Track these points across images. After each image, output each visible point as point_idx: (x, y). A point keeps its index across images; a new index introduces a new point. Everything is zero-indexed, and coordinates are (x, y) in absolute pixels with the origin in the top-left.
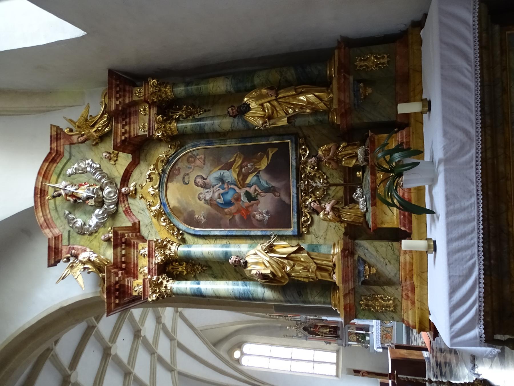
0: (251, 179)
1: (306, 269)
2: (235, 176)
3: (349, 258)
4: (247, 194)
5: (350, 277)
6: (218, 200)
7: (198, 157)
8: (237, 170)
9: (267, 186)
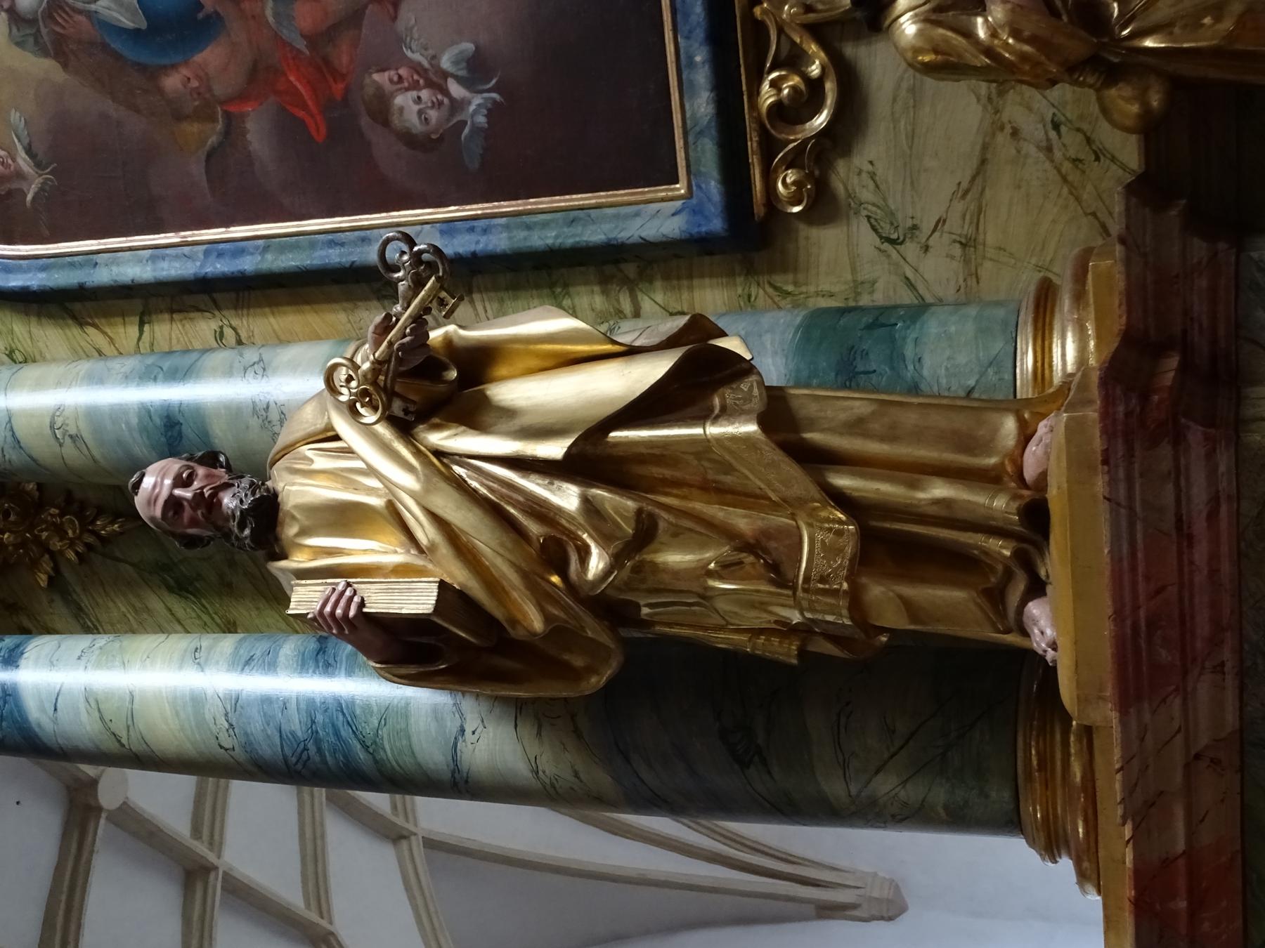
1: (768, 558)
3: (1195, 435)
5: (1203, 626)
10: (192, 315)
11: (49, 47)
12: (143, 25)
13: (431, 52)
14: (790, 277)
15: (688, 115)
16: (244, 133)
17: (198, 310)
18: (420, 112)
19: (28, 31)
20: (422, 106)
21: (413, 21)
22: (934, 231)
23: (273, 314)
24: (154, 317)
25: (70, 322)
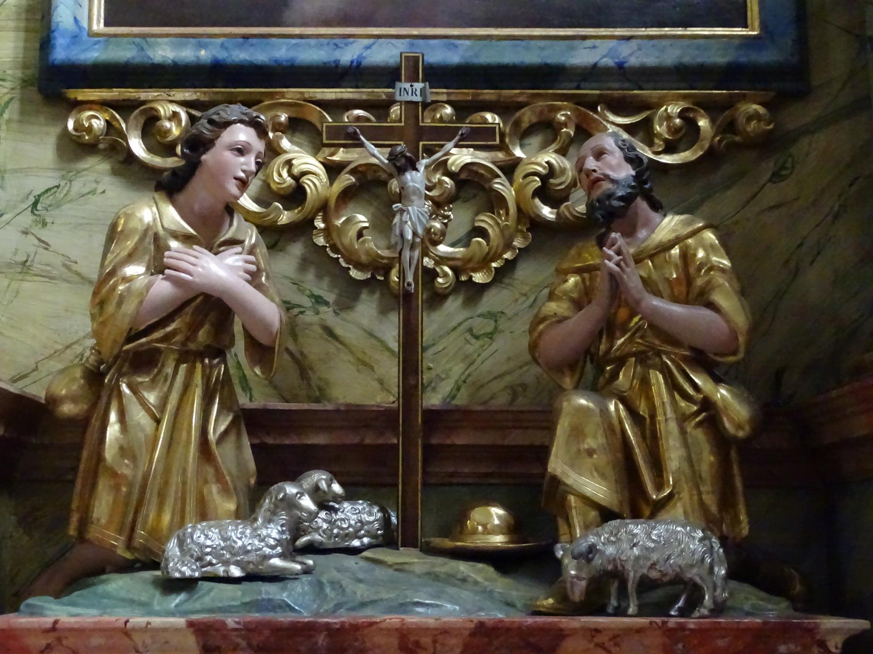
14: (16, 117)
22: (40, 240)
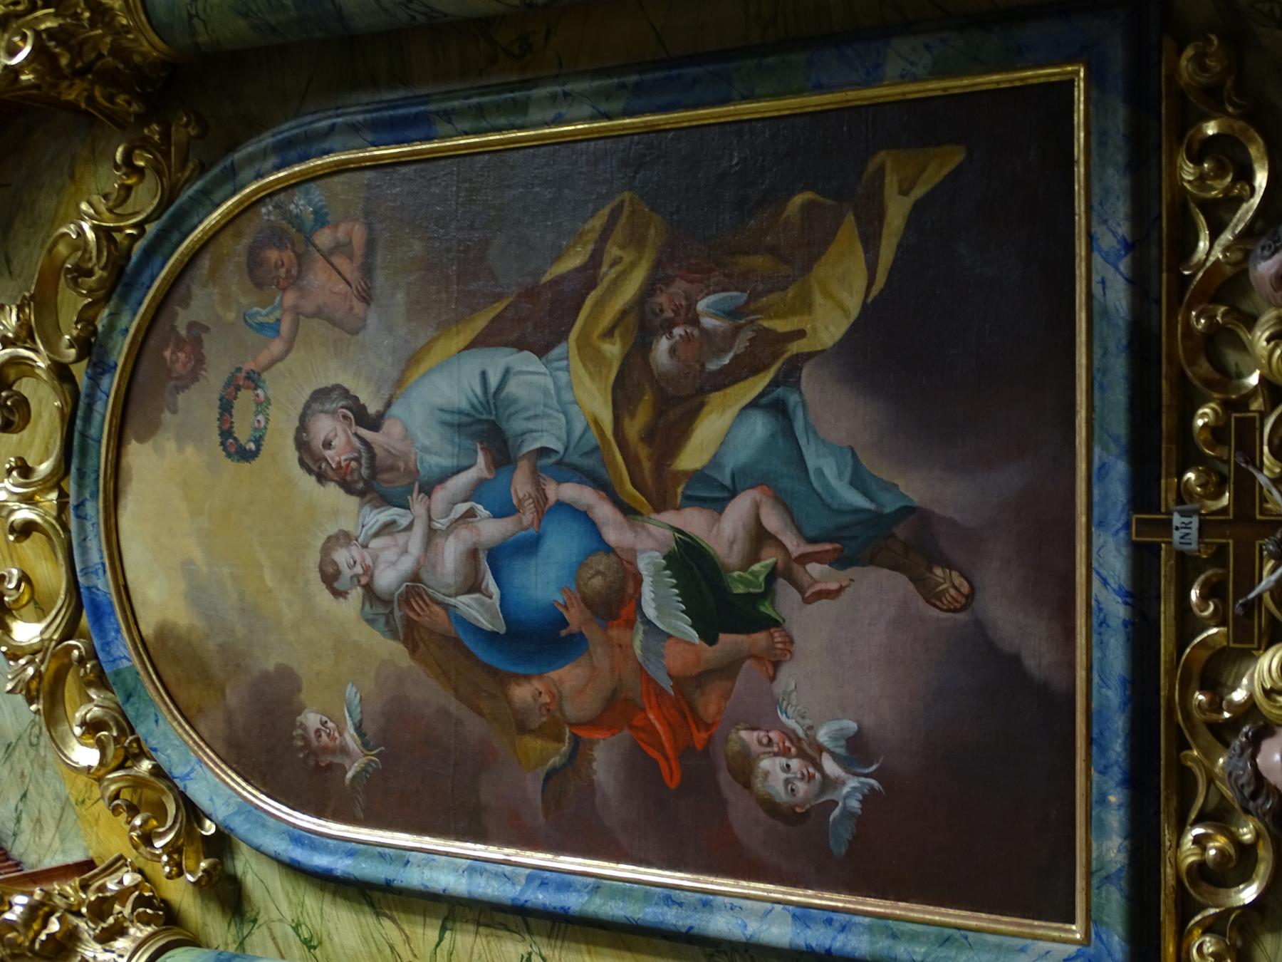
0: (720, 431)
2: (594, 401)
4: (689, 561)
6: (467, 604)
7: (324, 238)
8: (613, 350)
9: (856, 499)
10: (500, 933)
11: (400, 630)
12: (502, 629)
13: (808, 722)
15: (1094, 855)
16: (591, 761)
17: (507, 928)
18: (787, 781)
19: (381, 611)
20: (789, 775)
21: (792, 686)
23: (589, 952)
24: (458, 925)
25: (367, 909)
